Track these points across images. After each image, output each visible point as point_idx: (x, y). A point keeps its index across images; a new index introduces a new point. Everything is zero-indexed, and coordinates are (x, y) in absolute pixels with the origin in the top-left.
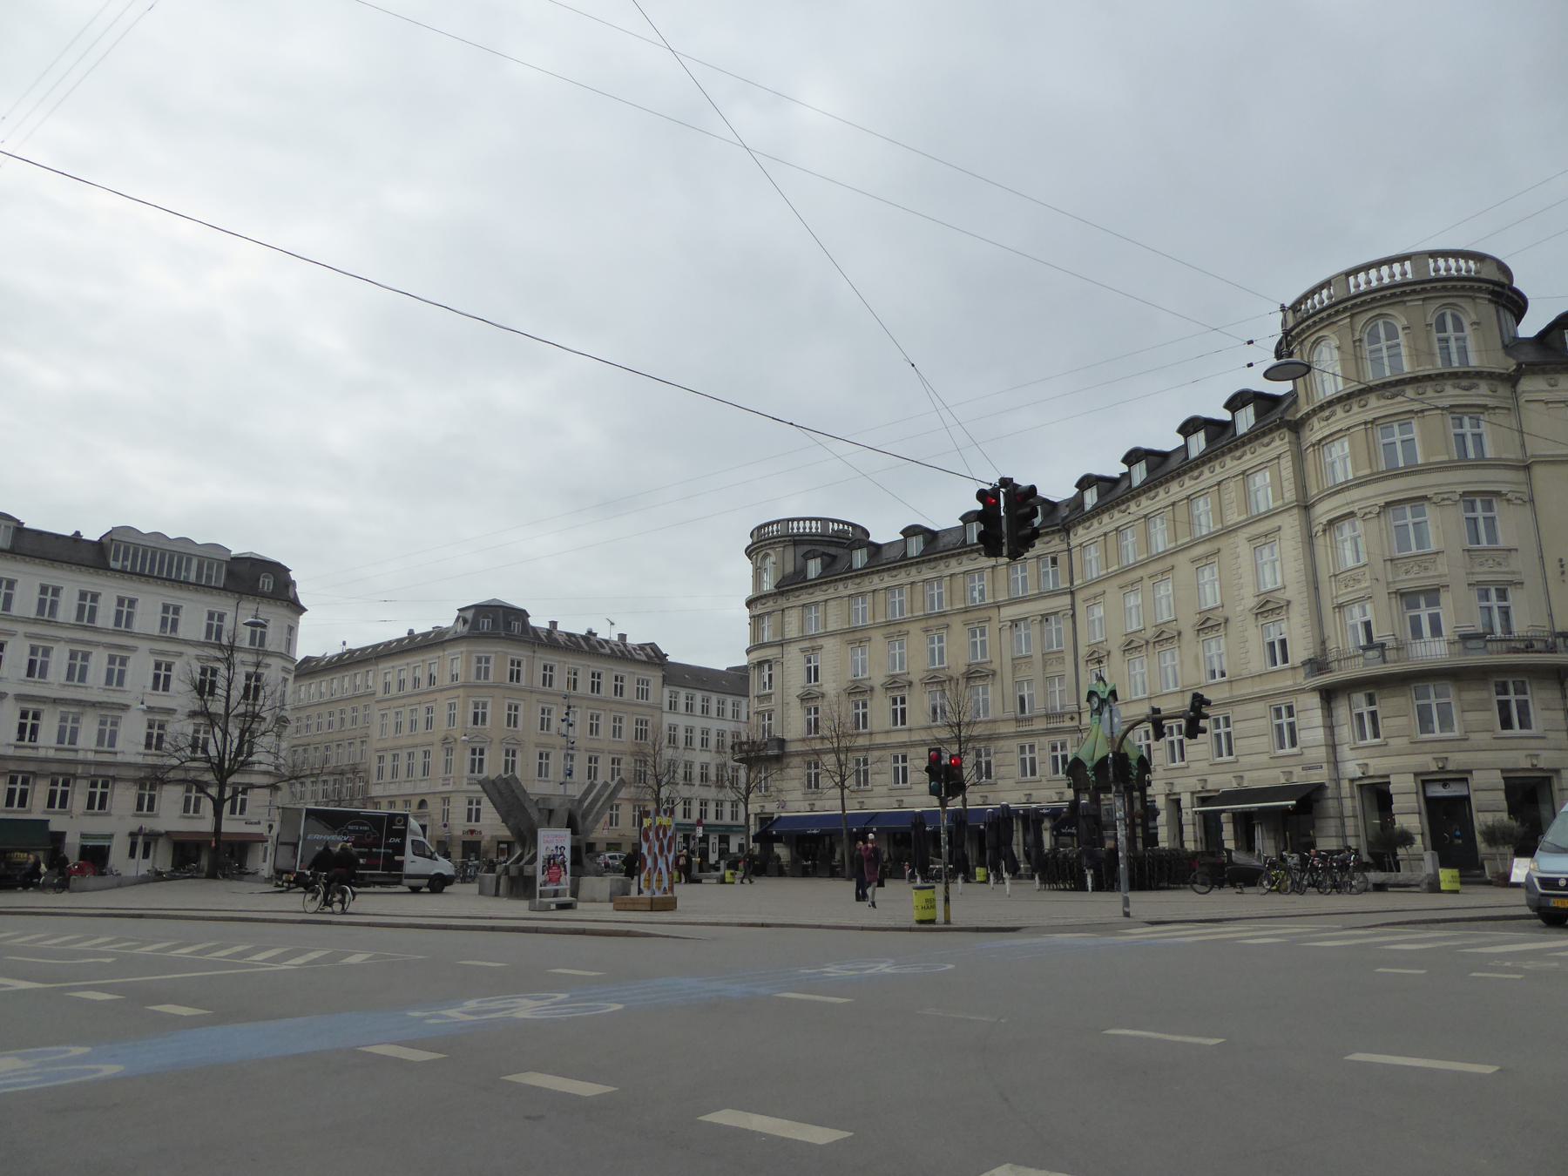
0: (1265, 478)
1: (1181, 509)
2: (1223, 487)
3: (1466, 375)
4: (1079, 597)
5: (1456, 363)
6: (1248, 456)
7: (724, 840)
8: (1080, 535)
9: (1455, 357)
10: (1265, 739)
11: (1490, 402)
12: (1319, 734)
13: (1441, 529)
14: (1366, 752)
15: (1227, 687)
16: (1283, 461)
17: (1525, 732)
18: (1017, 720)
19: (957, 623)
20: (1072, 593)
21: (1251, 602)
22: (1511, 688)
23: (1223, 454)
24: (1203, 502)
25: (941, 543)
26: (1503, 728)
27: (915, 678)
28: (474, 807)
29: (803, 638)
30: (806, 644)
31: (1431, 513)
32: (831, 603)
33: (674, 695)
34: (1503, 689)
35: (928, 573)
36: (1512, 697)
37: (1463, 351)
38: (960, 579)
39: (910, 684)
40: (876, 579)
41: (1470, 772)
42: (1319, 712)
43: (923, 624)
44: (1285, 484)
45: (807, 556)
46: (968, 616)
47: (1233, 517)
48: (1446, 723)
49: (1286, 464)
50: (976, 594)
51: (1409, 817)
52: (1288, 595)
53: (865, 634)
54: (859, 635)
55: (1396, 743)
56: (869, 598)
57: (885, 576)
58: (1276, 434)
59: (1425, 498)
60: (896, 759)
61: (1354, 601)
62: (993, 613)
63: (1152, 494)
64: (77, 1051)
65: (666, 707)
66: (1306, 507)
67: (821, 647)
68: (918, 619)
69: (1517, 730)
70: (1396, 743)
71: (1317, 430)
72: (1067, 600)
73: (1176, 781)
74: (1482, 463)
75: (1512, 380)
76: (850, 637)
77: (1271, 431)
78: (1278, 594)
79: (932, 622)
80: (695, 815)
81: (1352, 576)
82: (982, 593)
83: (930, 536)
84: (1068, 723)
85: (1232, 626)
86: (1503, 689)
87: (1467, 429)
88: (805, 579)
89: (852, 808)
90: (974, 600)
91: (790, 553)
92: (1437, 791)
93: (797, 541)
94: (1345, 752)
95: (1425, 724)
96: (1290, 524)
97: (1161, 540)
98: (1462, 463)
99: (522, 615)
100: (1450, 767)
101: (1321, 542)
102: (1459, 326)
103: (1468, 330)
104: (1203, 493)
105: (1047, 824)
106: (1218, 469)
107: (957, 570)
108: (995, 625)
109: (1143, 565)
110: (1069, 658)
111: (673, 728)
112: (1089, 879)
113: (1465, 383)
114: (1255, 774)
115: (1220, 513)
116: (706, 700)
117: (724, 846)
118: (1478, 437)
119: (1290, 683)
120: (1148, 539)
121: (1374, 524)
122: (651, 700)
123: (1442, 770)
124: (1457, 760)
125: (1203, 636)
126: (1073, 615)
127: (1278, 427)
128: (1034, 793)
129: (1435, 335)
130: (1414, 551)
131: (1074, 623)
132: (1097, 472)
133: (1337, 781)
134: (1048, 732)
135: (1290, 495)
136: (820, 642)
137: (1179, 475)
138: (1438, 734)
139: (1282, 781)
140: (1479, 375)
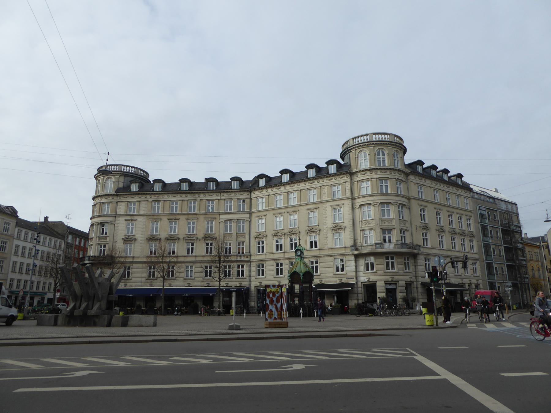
0: (340, 186)
1: (304, 193)
2: (322, 188)
3: (384, 169)
4: (254, 215)
5: (396, 166)
6: (333, 180)
7: (32, 299)
8: (256, 194)
9: (396, 164)
10: (332, 269)
11: (390, 177)
12: (353, 268)
13: (393, 212)
14: (369, 274)
15: (318, 251)
16: (346, 184)
17: (342, 273)
18: (237, 256)
19: (201, 218)
20: (250, 213)
21: (330, 225)
22: (390, 259)
23: (324, 178)
24: (314, 192)
26: (387, 269)
27: (181, 237)
28: (279, 267)
29: (127, 215)
30: (128, 218)
31: (372, 208)
33: (20, 231)
34: (387, 259)
35: (190, 197)
36: (390, 261)
37: (384, 162)
38: (204, 202)
39: (179, 239)
40: (166, 196)
41: (398, 281)
42: (354, 262)
43: (186, 217)
44: (347, 191)
45: (132, 182)
46: (207, 216)
47: (325, 198)
48: (393, 267)
49: (348, 186)
50: (210, 208)
51: (381, 294)
52: (344, 225)
54: (155, 217)
55: (380, 272)
56: (161, 204)
58: (345, 175)
59: (390, 203)
60: (239, 267)
61: (367, 230)
62: (217, 216)
63: (292, 185)
64: (518, 336)
65: (15, 237)
66: (353, 199)
67: (136, 220)
68: (184, 214)
70: (380, 272)
71: (357, 178)
72: (248, 215)
73: (281, 281)
74: (387, 194)
75: (407, 175)
76: (151, 217)
77: (344, 174)
78: (341, 224)
79: (190, 216)
80: (22, 287)
81: (369, 222)
82: (212, 208)
85: (321, 233)
86: (387, 259)
87: (384, 184)
88: (130, 191)
89: (167, 286)
90: (209, 210)
91: (122, 179)
92: (389, 287)
93: (126, 175)
94: (361, 274)
95: (388, 268)
96: (348, 203)
97: (294, 200)
98: (382, 194)
100: (371, 280)
101: (357, 211)
102: (383, 155)
103: (386, 155)
104: (314, 188)
105: (234, 294)
106: (321, 182)
107: (203, 198)
108: (218, 220)
109: (285, 208)
110: (247, 237)
111: (17, 246)
112: (301, 311)
113: (383, 171)
114: (327, 280)
115: (320, 195)
116: (26, 234)
117: (32, 301)
118: (386, 186)
119: (344, 252)
120: (288, 200)
121: (377, 208)
122: (10, 232)
123: (392, 281)
124: (396, 278)
125: (309, 234)
126: (250, 221)
127: (347, 173)
128: (230, 283)
129: (377, 157)
130: (386, 217)
131: (250, 224)
133: (357, 282)
134: (237, 261)
135: (348, 194)
136: (136, 218)
137: (305, 181)
138: (391, 270)
139: (338, 282)
140: (387, 169)
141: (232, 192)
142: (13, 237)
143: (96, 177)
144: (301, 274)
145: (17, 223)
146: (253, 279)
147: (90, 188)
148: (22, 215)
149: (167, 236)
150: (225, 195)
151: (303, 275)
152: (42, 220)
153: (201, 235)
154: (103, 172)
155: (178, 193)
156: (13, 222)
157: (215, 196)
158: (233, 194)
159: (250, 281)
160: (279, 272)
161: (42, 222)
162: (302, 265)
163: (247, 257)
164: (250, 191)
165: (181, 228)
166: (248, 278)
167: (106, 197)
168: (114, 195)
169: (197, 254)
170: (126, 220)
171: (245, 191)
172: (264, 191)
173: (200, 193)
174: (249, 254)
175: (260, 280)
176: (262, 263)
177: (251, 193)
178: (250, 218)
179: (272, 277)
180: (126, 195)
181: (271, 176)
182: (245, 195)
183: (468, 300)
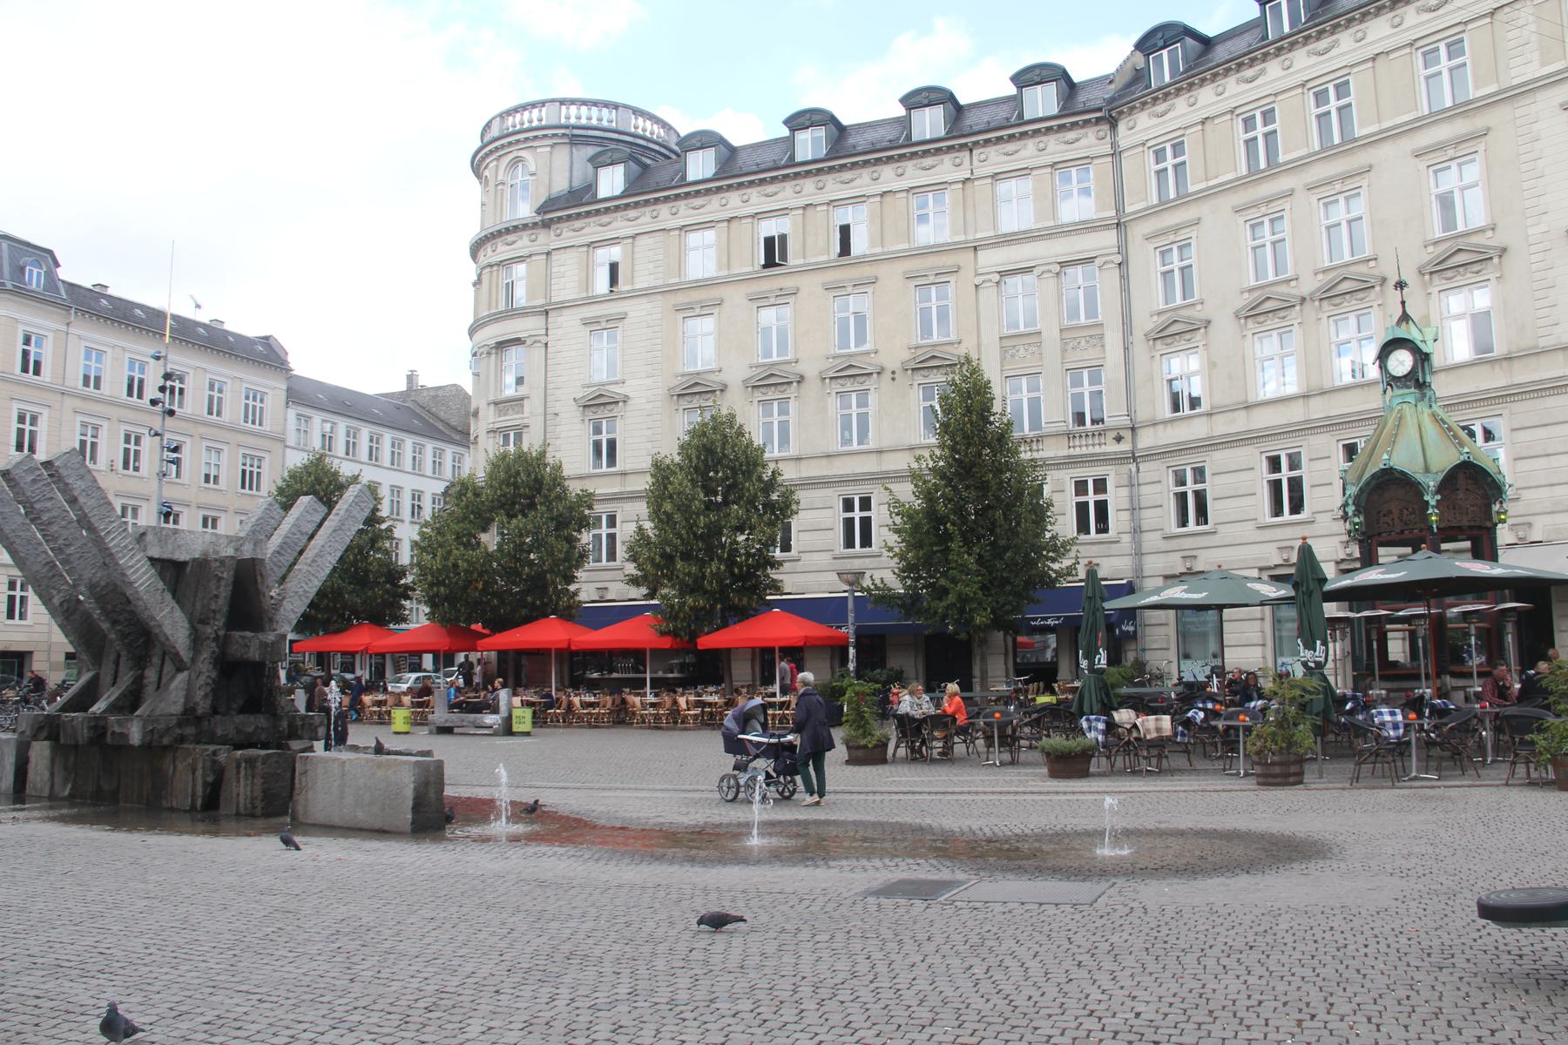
4: (1137, 232)
25: (971, 120)
27: (810, 369)
28: (857, 514)
32: (643, 241)
39: (801, 380)
45: (597, 163)
53: (715, 293)
57: (753, 193)
62: (965, 259)
63: (1323, 44)
69: (17, 621)
83: (839, 132)
84: (1112, 447)
91: (562, 155)
93: (575, 137)
99: (47, 258)
107: (895, 186)
108: (967, 278)
110: (1113, 339)
131: (1125, 278)
132: (57, 255)
141: (1024, 135)
142: (283, 441)
143: (477, 167)
144: (1431, 483)
145: (289, 390)
146: (1151, 541)
147: (463, 208)
148: (301, 365)
149: (748, 373)
150: (992, 152)
151: (1440, 489)
152: (403, 387)
153: (894, 355)
154: (496, 148)
155: (786, 177)
156: (274, 389)
157: (946, 168)
158: (1030, 146)
159: (1139, 554)
160: (1288, 496)
161: (401, 393)
162: (1431, 429)
163: (1119, 439)
164: (1110, 116)
165: (801, 326)
166: (1126, 538)
167: (510, 238)
168: (535, 224)
169: (885, 444)
170: (586, 323)
171: (1087, 122)
172: (1181, 104)
173: (878, 161)
174: (1126, 421)
175: (1188, 543)
176: (1195, 459)
177: (1113, 123)
178: (1122, 248)
179: (1250, 526)
180: (579, 216)
181: (1211, 34)
182: (1090, 141)
183: (781, 660)
